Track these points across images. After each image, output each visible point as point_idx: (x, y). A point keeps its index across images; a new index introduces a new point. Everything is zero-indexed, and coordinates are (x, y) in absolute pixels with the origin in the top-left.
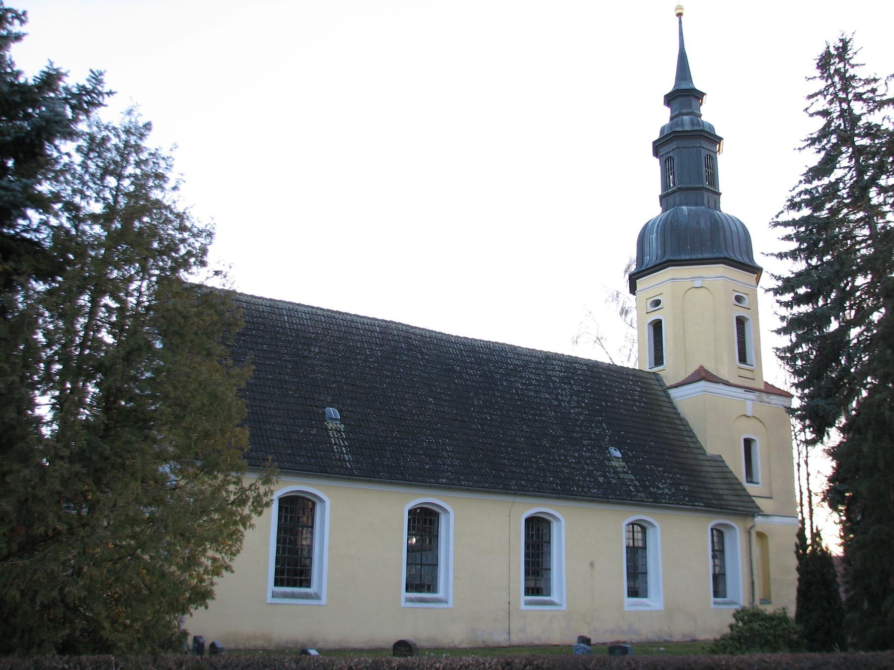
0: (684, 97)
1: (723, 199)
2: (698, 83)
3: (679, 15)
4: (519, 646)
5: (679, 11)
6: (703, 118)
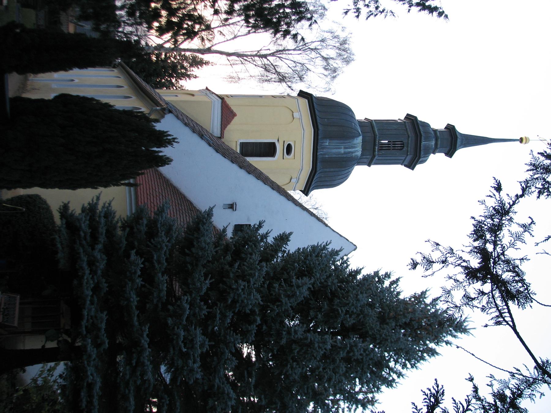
0: (451, 141)
1: (365, 167)
2: (460, 153)
3: (521, 140)
4: (181, 193)
5: (524, 141)
6: (432, 155)
